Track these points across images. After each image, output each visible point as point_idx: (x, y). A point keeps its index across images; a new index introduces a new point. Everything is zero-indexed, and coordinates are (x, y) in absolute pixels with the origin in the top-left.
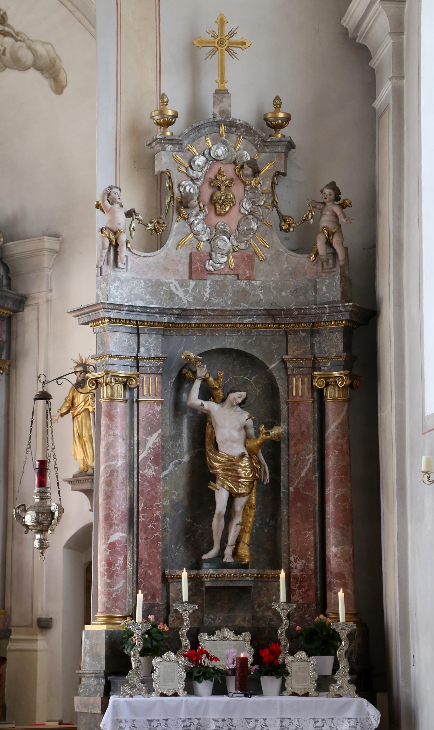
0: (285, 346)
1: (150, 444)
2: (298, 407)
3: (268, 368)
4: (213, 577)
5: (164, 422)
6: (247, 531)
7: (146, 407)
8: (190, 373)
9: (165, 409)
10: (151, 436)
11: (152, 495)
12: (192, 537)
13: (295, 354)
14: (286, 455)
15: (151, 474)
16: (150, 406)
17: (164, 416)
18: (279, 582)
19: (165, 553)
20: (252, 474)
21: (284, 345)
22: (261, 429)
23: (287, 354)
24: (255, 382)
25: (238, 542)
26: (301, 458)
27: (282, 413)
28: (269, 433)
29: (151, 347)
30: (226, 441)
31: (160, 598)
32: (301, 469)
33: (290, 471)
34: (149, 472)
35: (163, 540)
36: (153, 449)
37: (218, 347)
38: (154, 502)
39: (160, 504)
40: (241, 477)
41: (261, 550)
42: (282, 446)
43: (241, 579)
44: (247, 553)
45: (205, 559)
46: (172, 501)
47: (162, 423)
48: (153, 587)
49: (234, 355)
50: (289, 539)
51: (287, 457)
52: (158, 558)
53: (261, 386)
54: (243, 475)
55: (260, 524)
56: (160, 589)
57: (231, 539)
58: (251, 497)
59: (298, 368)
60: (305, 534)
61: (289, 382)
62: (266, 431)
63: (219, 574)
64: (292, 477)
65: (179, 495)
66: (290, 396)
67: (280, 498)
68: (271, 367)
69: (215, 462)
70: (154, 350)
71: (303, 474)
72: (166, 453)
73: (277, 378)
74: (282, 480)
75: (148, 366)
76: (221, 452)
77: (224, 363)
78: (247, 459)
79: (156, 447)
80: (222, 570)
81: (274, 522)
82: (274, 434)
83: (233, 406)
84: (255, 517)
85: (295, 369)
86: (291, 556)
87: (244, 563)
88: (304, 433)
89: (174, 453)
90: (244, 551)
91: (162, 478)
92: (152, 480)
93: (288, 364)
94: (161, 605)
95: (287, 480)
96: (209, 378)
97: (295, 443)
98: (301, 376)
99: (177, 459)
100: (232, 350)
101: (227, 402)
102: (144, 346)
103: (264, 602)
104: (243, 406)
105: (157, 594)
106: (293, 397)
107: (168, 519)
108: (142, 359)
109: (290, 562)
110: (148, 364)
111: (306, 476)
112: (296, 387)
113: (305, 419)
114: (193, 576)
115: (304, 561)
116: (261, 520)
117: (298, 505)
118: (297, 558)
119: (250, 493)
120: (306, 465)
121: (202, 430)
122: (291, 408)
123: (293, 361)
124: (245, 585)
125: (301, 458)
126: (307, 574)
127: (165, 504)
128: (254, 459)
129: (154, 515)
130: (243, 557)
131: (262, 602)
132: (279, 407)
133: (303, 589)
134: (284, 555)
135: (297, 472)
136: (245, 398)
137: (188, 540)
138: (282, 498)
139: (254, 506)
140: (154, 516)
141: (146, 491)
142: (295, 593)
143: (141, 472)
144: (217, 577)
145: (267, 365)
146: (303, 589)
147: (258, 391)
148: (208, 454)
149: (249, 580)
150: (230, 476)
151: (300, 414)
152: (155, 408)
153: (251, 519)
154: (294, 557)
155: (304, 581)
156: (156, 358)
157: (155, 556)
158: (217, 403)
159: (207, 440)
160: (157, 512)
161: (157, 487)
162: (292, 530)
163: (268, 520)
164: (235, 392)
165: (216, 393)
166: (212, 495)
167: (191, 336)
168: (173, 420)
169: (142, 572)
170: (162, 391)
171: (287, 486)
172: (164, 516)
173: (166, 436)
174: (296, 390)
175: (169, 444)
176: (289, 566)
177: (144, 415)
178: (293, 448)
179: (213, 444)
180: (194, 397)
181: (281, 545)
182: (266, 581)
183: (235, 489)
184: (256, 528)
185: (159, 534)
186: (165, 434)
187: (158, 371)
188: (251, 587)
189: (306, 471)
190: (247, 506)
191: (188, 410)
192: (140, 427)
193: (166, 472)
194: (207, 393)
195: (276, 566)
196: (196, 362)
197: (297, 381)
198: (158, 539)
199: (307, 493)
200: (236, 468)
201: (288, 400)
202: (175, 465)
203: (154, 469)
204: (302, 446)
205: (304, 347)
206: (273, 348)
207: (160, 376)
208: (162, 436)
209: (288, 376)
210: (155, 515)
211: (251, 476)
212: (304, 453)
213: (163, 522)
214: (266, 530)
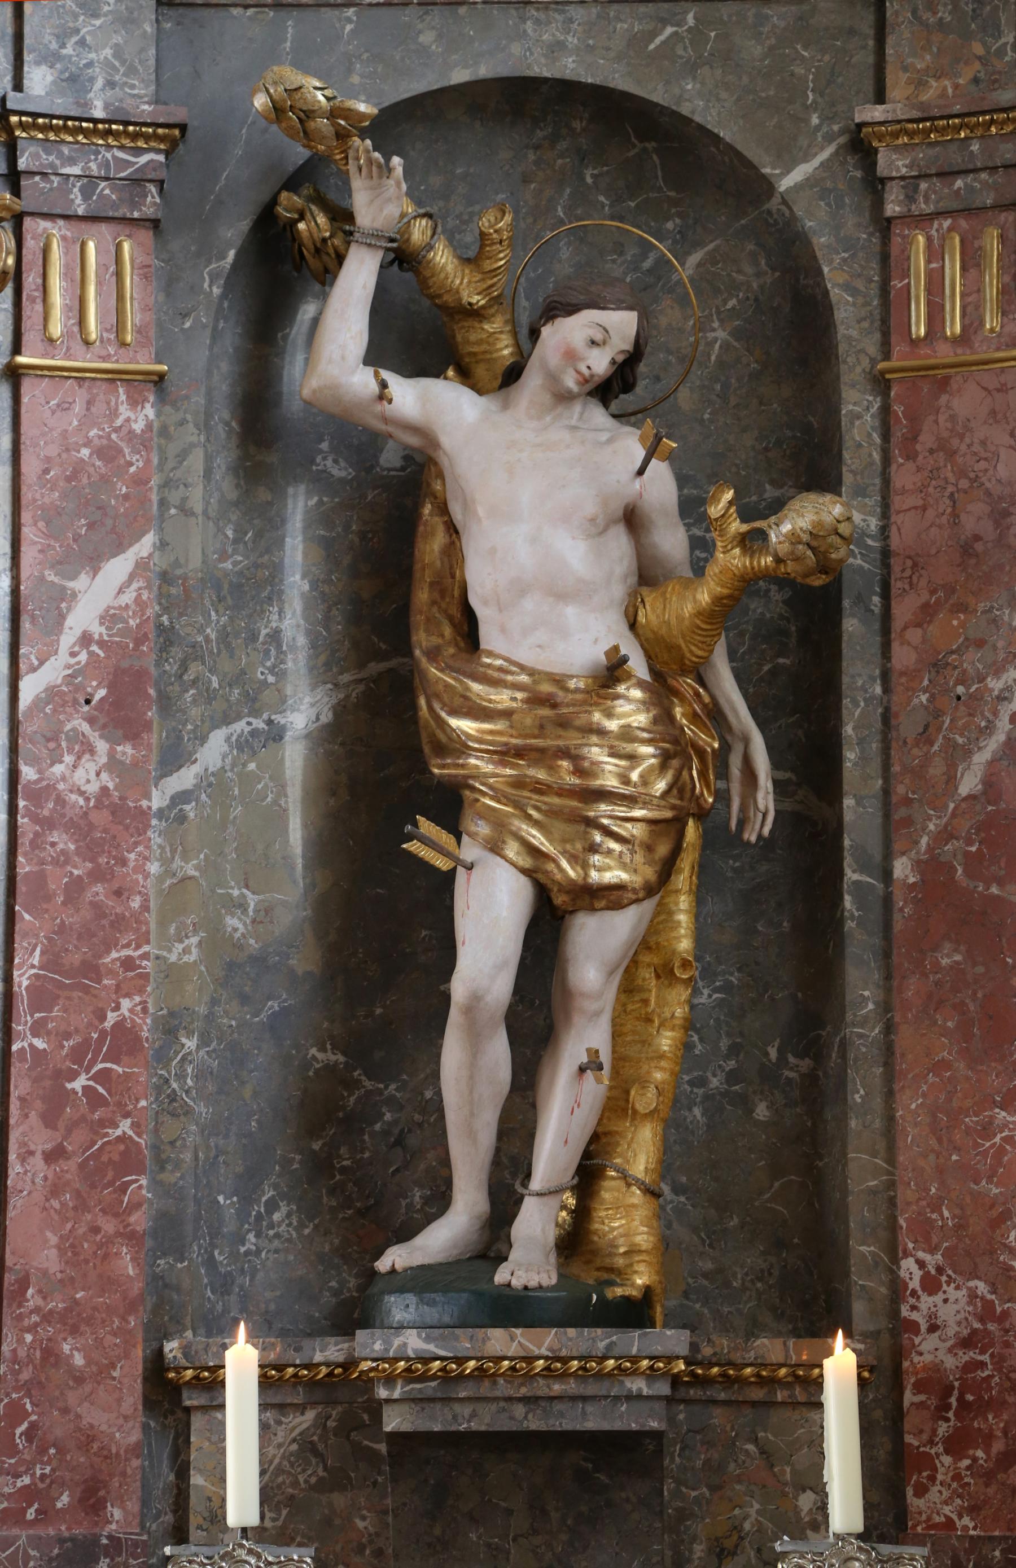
0: (871, 59)
1: (84, 617)
2: (944, 399)
3: (768, 186)
4: (424, 1378)
5: (174, 497)
6: (640, 1108)
7: (65, 407)
8: (321, 219)
9: (182, 423)
10: (95, 571)
11: (95, 905)
12: (343, 1151)
13: (924, 98)
14: (873, 679)
15: (93, 788)
16: (90, 403)
17: (171, 464)
18: (820, 1406)
19: (168, 1234)
20: (670, 775)
21: (866, 58)
22: (715, 511)
23: (880, 98)
24: (706, 281)
25: (588, 1174)
26: (960, 690)
27: (848, 443)
28: (762, 535)
29: (90, 64)
30: (521, 589)
31: (133, 1506)
32: (957, 755)
33: (896, 768)
34: (80, 776)
35: (161, 1164)
36: (101, 643)
37: (484, 72)
38: (110, 945)
39: (145, 956)
40: (603, 795)
41: (735, 1221)
42: (851, 625)
43: (591, 1389)
44: (644, 1238)
45: (393, 1271)
46: (216, 941)
47: (163, 503)
48: (91, 1439)
49: (577, 125)
50: (891, 1159)
51: (878, 690)
52: (127, 1265)
53: (732, 303)
54: (611, 783)
55: (732, 1077)
56: (135, 1450)
57: (553, 1154)
58: (671, 913)
59: (939, 175)
60: (987, 1130)
61: (888, 264)
62: (745, 528)
63: (460, 1361)
64: (907, 802)
65: (267, 911)
66: (894, 339)
67: (841, 922)
68: (786, 183)
69: (454, 712)
70: (111, 84)
71: (969, 783)
72: (184, 667)
73: (821, 241)
74: (848, 817)
75: (76, 170)
76: (490, 654)
77: (526, 180)
78: (637, 694)
79: (121, 633)
80: (480, 1332)
81: (806, 1064)
82: (794, 538)
83: (563, 398)
84: (690, 1025)
85: (923, 186)
86: (906, 1254)
87: (619, 1291)
88: (979, 547)
89: (239, 678)
90: (627, 1222)
91: (161, 814)
92: (95, 817)
93: (882, 159)
94: (136, 1544)
95: (879, 821)
96: (430, 247)
97: (926, 606)
98: (963, 223)
99: (255, 713)
100: (566, 92)
101: (532, 380)
102: (50, 59)
103: (747, 1526)
104: (624, 401)
105: (115, 1482)
106: (915, 343)
107: (190, 1044)
108: (35, 126)
109: (897, 1290)
110: (71, 161)
111: (985, 793)
112: (929, 291)
113: (983, 465)
114: (324, 1370)
115: (981, 1287)
116: (734, 1050)
117: (945, 962)
118: (940, 1270)
119: (659, 884)
120: (989, 729)
121: (394, 535)
122: (898, 409)
123: (911, 134)
124: (618, 1426)
125: (960, 690)
126: (999, 1361)
127: (173, 958)
128: (682, 699)
129: (103, 1018)
130: (620, 1262)
131: (737, 1528)
132: (832, 411)
133: (980, 1454)
134: (864, 1249)
135: (937, 770)
136: (628, 346)
137: (320, 1167)
138: (850, 925)
139: (685, 964)
140: (108, 1024)
141: (57, 882)
142: (932, 1478)
143: (28, 773)
144: (446, 1377)
145: (767, 170)
146: (980, 1454)
147: (721, 334)
148: (423, 674)
149: (639, 1397)
150: (540, 789)
151: (955, 442)
152: (115, 413)
153: (666, 1041)
154: (921, 1264)
155: (983, 1407)
156: (119, 128)
157: (106, 1256)
158: (480, 392)
159: (422, 596)
160: (126, 1004)
161: (124, 862)
162: (910, 1105)
163: (773, 1053)
164: (571, 309)
165: (473, 337)
166: (435, 896)
167: (327, 13)
168: (233, 495)
169: (22, 1353)
170: (160, 324)
171: (876, 853)
172: (170, 1028)
173: (185, 578)
174: (929, 303)
175: (209, 625)
176: (894, 1314)
177: (53, 450)
178: (914, 635)
179: (451, 619)
180: (337, 345)
181: (845, 1193)
182: (754, 1404)
183: (564, 864)
184: (707, 1097)
185: (135, 1126)
186: (177, 564)
187: (134, 205)
188: (657, 1436)
189: (991, 763)
190: (642, 966)
191: (324, 446)
192: (26, 517)
193: (185, 778)
194: (418, 334)
195: (818, 1315)
196: (342, 136)
197: (935, 253)
198: (128, 1159)
199: (994, 890)
200: (571, 739)
201: (882, 365)
202: (243, 745)
203: (111, 754)
204: (963, 625)
205: (978, 49)
206: (800, 71)
207: (146, 236)
208: (165, 577)
209: (884, 226)
210: (111, 1018)
211: (660, 786)
212: (972, 661)
213: (162, 1057)
214: (762, 1111)
